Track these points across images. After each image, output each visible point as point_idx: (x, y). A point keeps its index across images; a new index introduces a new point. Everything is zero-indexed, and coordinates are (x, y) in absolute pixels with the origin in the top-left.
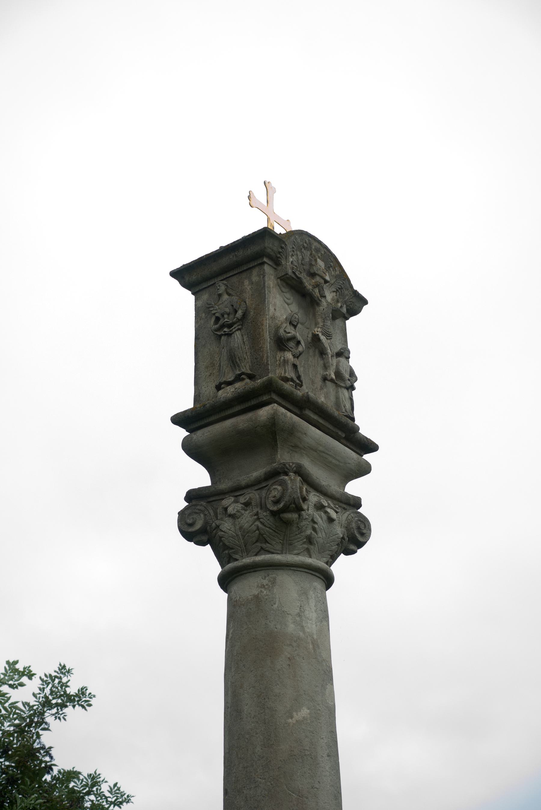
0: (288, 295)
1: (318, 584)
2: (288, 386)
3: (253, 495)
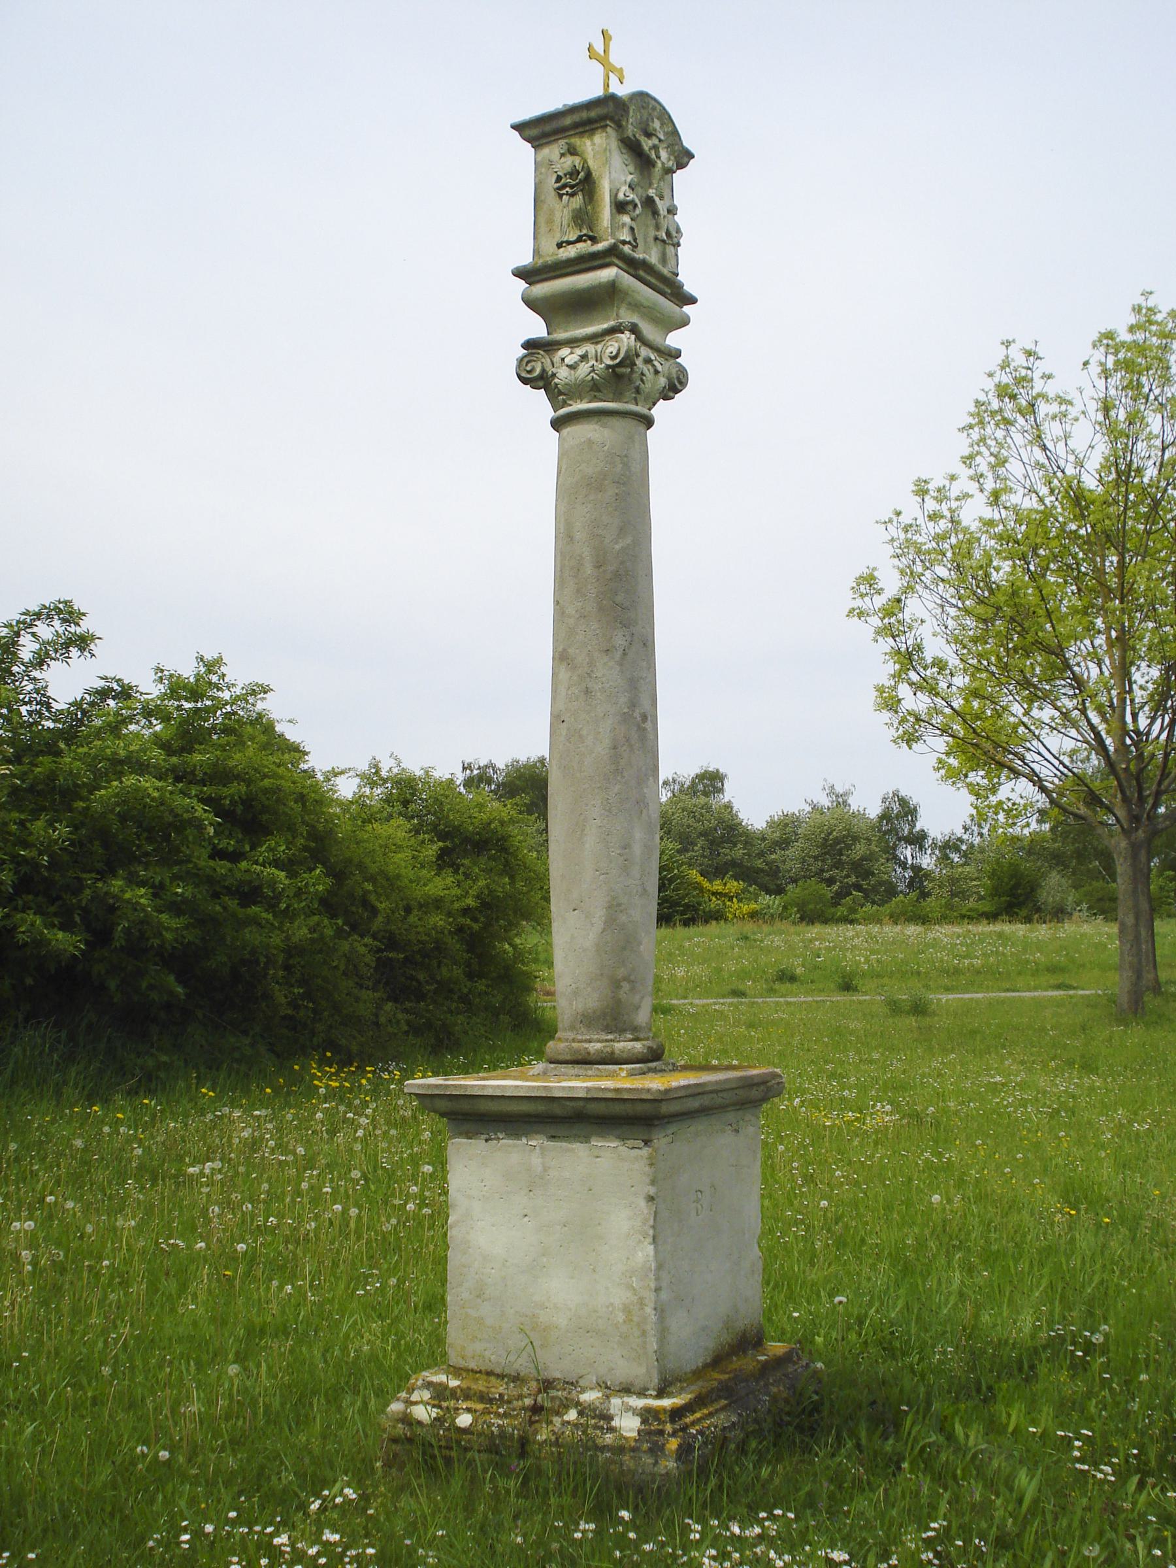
0: (626, 156)
1: (642, 428)
2: (627, 249)
3: (590, 348)
